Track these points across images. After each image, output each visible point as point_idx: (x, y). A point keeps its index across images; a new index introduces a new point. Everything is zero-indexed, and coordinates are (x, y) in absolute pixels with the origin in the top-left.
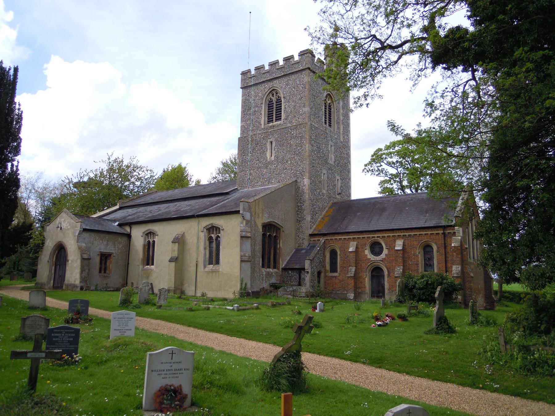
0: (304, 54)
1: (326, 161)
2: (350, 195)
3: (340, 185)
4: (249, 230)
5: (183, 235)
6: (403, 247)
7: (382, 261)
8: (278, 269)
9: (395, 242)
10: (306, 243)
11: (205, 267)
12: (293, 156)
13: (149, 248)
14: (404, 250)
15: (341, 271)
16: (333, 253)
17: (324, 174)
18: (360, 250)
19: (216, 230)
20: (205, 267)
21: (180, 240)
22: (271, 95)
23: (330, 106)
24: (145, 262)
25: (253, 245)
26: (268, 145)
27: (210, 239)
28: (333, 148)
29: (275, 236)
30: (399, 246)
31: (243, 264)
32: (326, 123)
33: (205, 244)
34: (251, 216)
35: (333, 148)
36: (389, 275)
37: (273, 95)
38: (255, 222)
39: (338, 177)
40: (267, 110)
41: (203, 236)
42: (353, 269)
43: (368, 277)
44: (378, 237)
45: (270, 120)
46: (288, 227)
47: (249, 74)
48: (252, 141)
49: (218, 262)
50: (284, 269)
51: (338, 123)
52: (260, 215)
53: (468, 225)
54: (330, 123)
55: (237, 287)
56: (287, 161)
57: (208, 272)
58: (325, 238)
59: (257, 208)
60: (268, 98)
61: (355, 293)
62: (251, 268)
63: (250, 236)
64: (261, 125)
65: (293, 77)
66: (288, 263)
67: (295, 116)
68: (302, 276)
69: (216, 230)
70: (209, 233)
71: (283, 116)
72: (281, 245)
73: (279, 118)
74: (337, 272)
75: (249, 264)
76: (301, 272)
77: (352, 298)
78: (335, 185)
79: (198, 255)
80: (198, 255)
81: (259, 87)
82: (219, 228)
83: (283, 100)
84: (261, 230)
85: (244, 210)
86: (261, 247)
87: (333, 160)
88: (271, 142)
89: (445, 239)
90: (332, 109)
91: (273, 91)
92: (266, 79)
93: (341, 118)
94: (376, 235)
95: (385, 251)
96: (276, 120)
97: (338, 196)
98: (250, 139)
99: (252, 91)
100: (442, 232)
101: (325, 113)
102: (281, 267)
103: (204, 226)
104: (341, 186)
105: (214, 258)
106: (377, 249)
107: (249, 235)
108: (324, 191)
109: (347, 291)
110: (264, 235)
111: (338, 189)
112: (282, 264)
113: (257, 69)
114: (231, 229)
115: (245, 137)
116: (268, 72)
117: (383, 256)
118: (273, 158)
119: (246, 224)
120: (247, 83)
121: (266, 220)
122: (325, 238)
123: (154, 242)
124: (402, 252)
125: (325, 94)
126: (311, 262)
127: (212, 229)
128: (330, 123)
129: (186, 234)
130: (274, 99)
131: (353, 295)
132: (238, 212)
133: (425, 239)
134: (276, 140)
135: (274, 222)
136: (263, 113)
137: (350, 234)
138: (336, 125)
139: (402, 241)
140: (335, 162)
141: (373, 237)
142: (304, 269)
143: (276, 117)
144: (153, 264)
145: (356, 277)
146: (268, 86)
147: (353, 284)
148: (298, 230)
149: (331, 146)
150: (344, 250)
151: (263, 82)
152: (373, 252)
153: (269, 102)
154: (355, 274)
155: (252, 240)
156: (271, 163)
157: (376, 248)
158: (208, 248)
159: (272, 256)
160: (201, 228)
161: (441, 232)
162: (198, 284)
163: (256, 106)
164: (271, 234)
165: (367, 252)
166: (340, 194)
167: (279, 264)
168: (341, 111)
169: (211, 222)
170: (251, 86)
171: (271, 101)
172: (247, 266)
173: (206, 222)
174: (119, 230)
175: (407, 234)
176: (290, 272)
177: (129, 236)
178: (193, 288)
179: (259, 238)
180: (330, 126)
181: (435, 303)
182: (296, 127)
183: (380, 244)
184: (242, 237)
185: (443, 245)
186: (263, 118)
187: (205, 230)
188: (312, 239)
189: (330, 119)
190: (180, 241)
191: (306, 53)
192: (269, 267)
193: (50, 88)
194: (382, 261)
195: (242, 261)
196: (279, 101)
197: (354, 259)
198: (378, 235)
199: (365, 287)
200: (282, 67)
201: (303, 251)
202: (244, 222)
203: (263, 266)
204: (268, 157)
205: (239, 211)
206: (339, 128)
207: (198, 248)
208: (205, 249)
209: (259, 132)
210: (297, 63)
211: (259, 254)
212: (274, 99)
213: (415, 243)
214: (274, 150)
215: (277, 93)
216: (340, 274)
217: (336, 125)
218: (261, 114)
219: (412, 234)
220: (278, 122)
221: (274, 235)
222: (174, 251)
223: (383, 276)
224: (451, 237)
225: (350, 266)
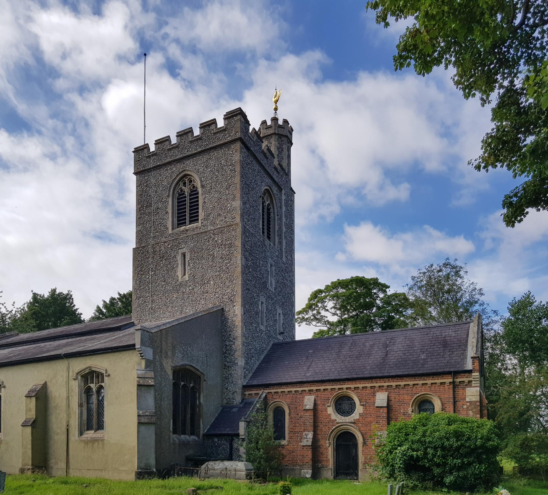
0: (233, 116)
2: (294, 336)
3: (282, 322)
4: (151, 374)
5: (45, 386)
6: (388, 404)
7: (354, 423)
8: (198, 436)
9: (374, 395)
10: (238, 399)
11: (81, 433)
12: (217, 273)
14: (389, 407)
15: (291, 438)
16: (279, 413)
17: (262, 303)
18: (320, 407)
19: (98, 377)
20: (81, 433)
21: (41, 396)
22: (181, 184)
23: (268, 209)
25: (158, 401)
26: (179, 258)
27: (88, 391)
28: (273, 268)
29: (193, 387)
30: (381, 399)
31: (143, 428)
32: (263, 232)
33: (80, 398)
35: (273, 268)
36: (364, 443)
37: (185, 184)
38: (161, 364)
39: (280, 311)
40: (176, 220)
41: (76, 386)
42: (310, 435)
43: (332, 446)
44: (347, 388)
45: (181, 221)
46: (211, 376)
47: (146, 150)
48: (154, 252)
49: (100, 426)
50: (207, 436)
51: (280, 236)
52: (170, 353)
54: (269, 234)
55: (134, 466)
57: (87, 442)
58: (266, 391)
59: (164, 343)
60: (178, 190)
61: (313, 469)
62: (156, 434)
63: (153, 383)
64: (167, 228)
65: (216, 153)
66: (214, 425)
67: (220, 215)
68: (235, 446)
69: (98, 377)
70: (86, 382)
72: (201, 401)
73: (194, 218)
74: (285, 439)
75: (152, 429)
76: (233, 440)
77: (308, 476)
78: (276, 320)
79: (69, 415)
80: (69, 415)
81: (162, 171)
82: (102, 374)
83: (200, 190)
84: (171, 377)
85: (143, 343)
86: (171, 402)
87: (274, 286)
88: (184, 255)
89: (454, 391)
90: (272, 214)
91: (185, 178)
92: (173, 159)
93: (284, 230)
94: (345, 386)
95: (359, 409)
96: (191, 222)
97: (279, 337)
98: (151, 250)
99: (152, 178)
100: (451, 380)
101: (263, 215)
102: (201, 433)
103: (76, 371)
104: (283, 323)
105: (93, 418)
106: (345, 406)
107: (151, 382)
108: (262, 328)
109: (300, 466)
110: (176, 385)
111: (279, 327)
112: (203, 429)
113: (159, 143)
114: (123, 377)
115: (144, 247)
116: (176, 147)
117: (355, 416)
118: (187, 277)
119: (147, 366)
121: (179, 362)
122: (266, 391)
124: (385, 410)
125: (264, 188)
126: (247, 426)
127: (90, 376)
128: (269, 234)
129: (48, 384)
130: (187, 190)
131: (310, 471)
133: (422, 391)
134: (192, 251)
135: (191, 366)
136: (170, 212)
137: (305, 385)
138: (277, 238)
139: (386, 394)
140: (275, 289)
141: (339, 389)
142: (238, 435)
143: (190, 218)
145: (315, 446)
146: (176, 169)
147: (310, 456)
148: (226, 379)
149: (271, 265)
150: (295, 405)
151: (170, 163)
152: (340, 410)
153: (180, 195)
154: (313, 442)
155: (156, 391)
157: (344, 405)
158: (85, 405)
159: (189, 416)
160: (72, 375)
161: (448, 380)
162: (71, 460)
164: (185, 386)
165: (331, 410)
166: (282, 333)
167: (199, 429)
168: (284, 220)
169: (88, 365)
170: (149, 170)
171: (182, 193)
172: (150, 432)
173: (80, 365)
175: (394, 384)
176: (216, 440)
178: (64, 466)
179: (168, 390)
180: (269, 238)
182: (221, 231)
183: (350, 399)
184: (139, 386)
185: (452, 400)
186: (170, 219)
187: (80, 377)
188: (247, 393)
189: (269, 228)
190: (41, 396)
191: (236, 115)
192: (184, 433)
194: (354, 423)
195: (140, 423)
196: (194, 193)
197: (312, 421)
198: (349, 386)
199: (328, 461)
200: (199, 138)
201: (235, 410)
202: (143, 363)
203: (175, 432)
204: (180, 276)
205: (134, 345)
206: (280, 243)
207: (68, 406)
208: (81, 405)
209: (164, 239)
210: (223, 130)
211: (168, 413)
212: (187, 190)
213: (406, 397)
214: (189, 265)
215: (191, 181)
216: (289, 442)
217: (277, 238)
218: (167, 213)
219: (402, 383)
220: (194, 225)
221: (191, 385)
222: (30, 410)
223: (356, 446)
224: (464, 389)
225: (304, 430)
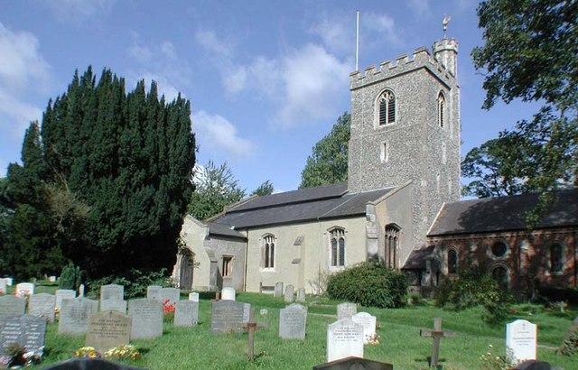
1: (440, 164)
13: (269, 250)
24: (264, 264)
27: (334, 241)
34: (376, 218)
45: (382, 121)
53: (55, 106)
56: (402, 163)
71: (397, 117)
73: (392, 119)
120: (357, 85)
123: (273, 245)
127: (270, 236)
132: (364, 215)
144: (272, 266)
156: (384, 165)
163: (368, 108)
174: (235, 233)
177: (246, 240)
179: (383, 239)
181: (520, 84)
193: (90, 68)
